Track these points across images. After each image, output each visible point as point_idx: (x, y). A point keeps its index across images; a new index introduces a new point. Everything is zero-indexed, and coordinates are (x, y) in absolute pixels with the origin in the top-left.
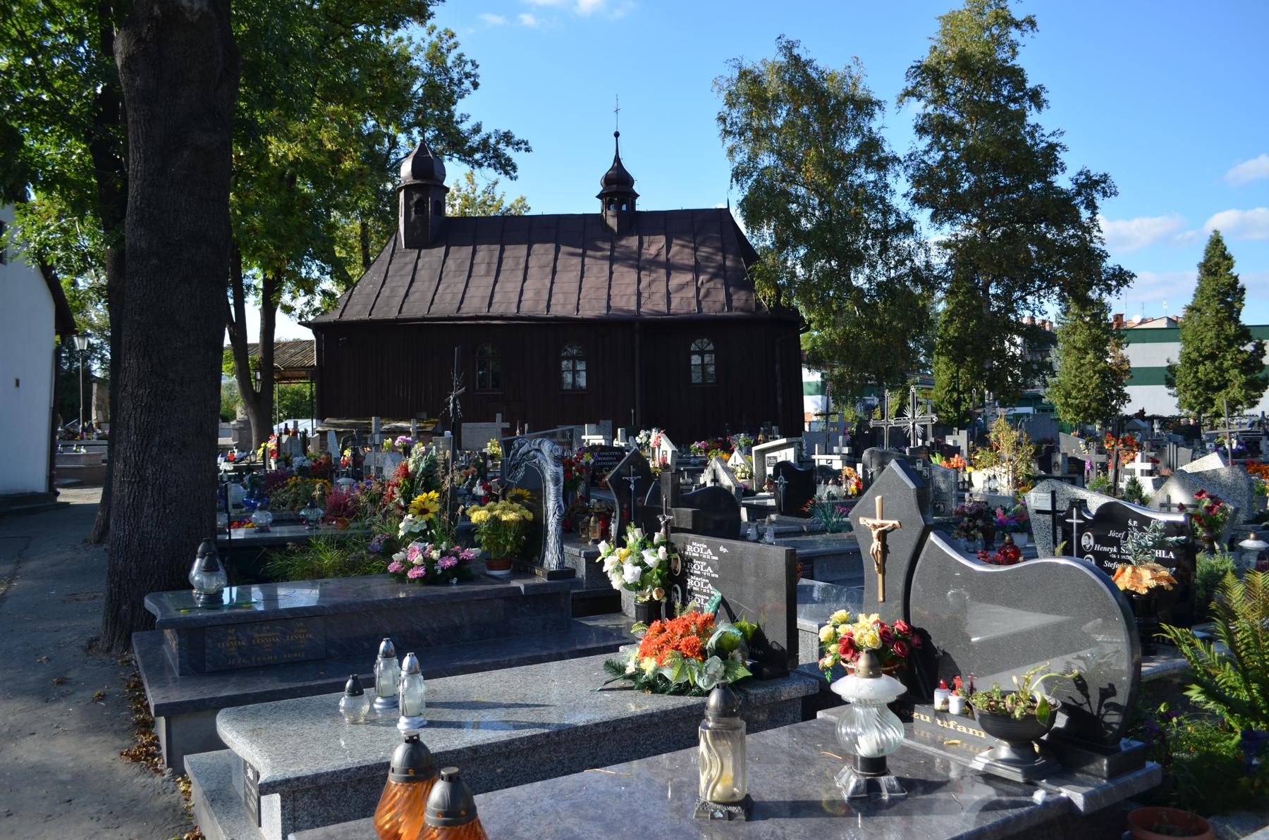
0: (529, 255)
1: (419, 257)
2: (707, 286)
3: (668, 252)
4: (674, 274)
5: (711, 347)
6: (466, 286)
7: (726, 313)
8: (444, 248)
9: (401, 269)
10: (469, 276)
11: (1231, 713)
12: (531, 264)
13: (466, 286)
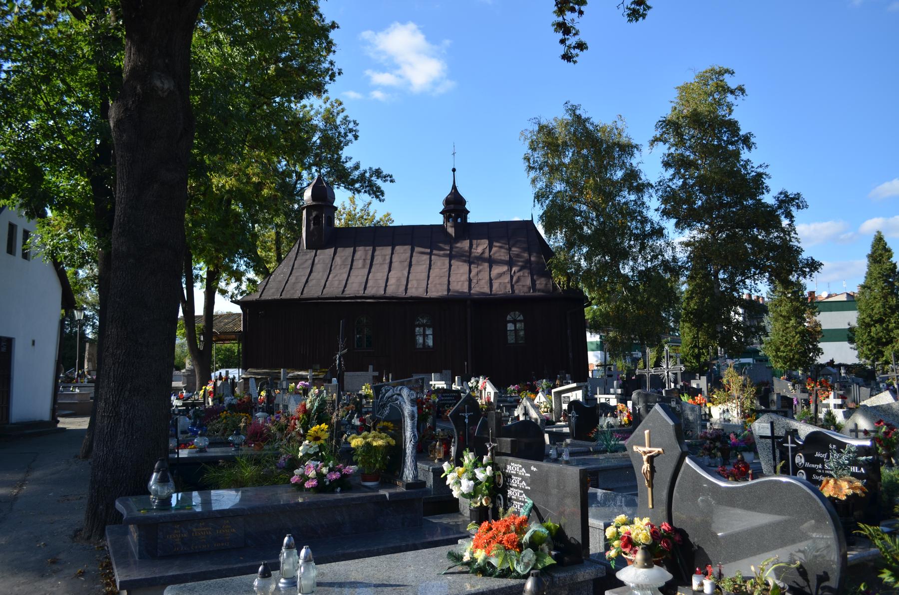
0: (392, 253)
1: (316, 255)
2: (518, 274)
7: (531, 293)
10: (351, 269)
12: (394, 260)
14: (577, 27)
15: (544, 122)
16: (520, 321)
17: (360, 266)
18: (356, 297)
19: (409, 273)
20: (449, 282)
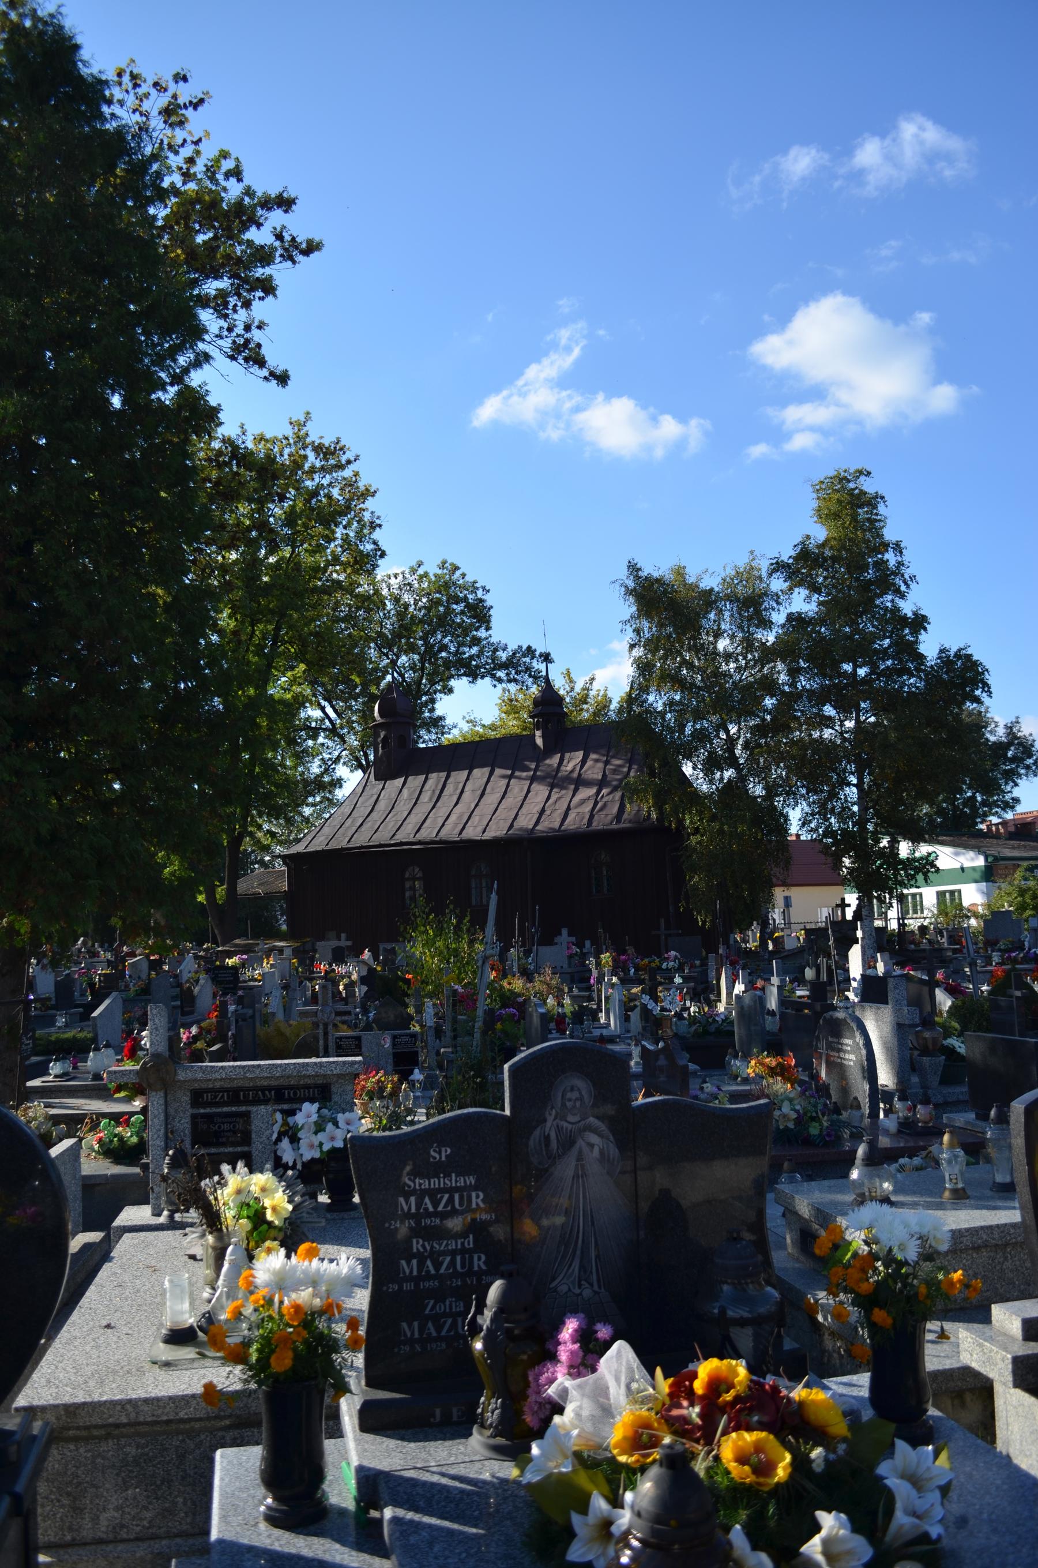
0: (467, 779)
1: (383, 788)
2: (605, 799)
3: (581, 768)
4: (581, 789)
5: (420, 875)
6: (409, 814)
7: (614, 826)
8: (466, 772)
9: (367, 800)
10: (415, 803)
11: (447, 1175)
12: (466, 789)
13: (409, 814)
14: (319, 432)
15: (649, 569)
16: (419, 879)
17: (426, 799)
18: (362, 847)
19: (477, 805)
20: (517, 814)
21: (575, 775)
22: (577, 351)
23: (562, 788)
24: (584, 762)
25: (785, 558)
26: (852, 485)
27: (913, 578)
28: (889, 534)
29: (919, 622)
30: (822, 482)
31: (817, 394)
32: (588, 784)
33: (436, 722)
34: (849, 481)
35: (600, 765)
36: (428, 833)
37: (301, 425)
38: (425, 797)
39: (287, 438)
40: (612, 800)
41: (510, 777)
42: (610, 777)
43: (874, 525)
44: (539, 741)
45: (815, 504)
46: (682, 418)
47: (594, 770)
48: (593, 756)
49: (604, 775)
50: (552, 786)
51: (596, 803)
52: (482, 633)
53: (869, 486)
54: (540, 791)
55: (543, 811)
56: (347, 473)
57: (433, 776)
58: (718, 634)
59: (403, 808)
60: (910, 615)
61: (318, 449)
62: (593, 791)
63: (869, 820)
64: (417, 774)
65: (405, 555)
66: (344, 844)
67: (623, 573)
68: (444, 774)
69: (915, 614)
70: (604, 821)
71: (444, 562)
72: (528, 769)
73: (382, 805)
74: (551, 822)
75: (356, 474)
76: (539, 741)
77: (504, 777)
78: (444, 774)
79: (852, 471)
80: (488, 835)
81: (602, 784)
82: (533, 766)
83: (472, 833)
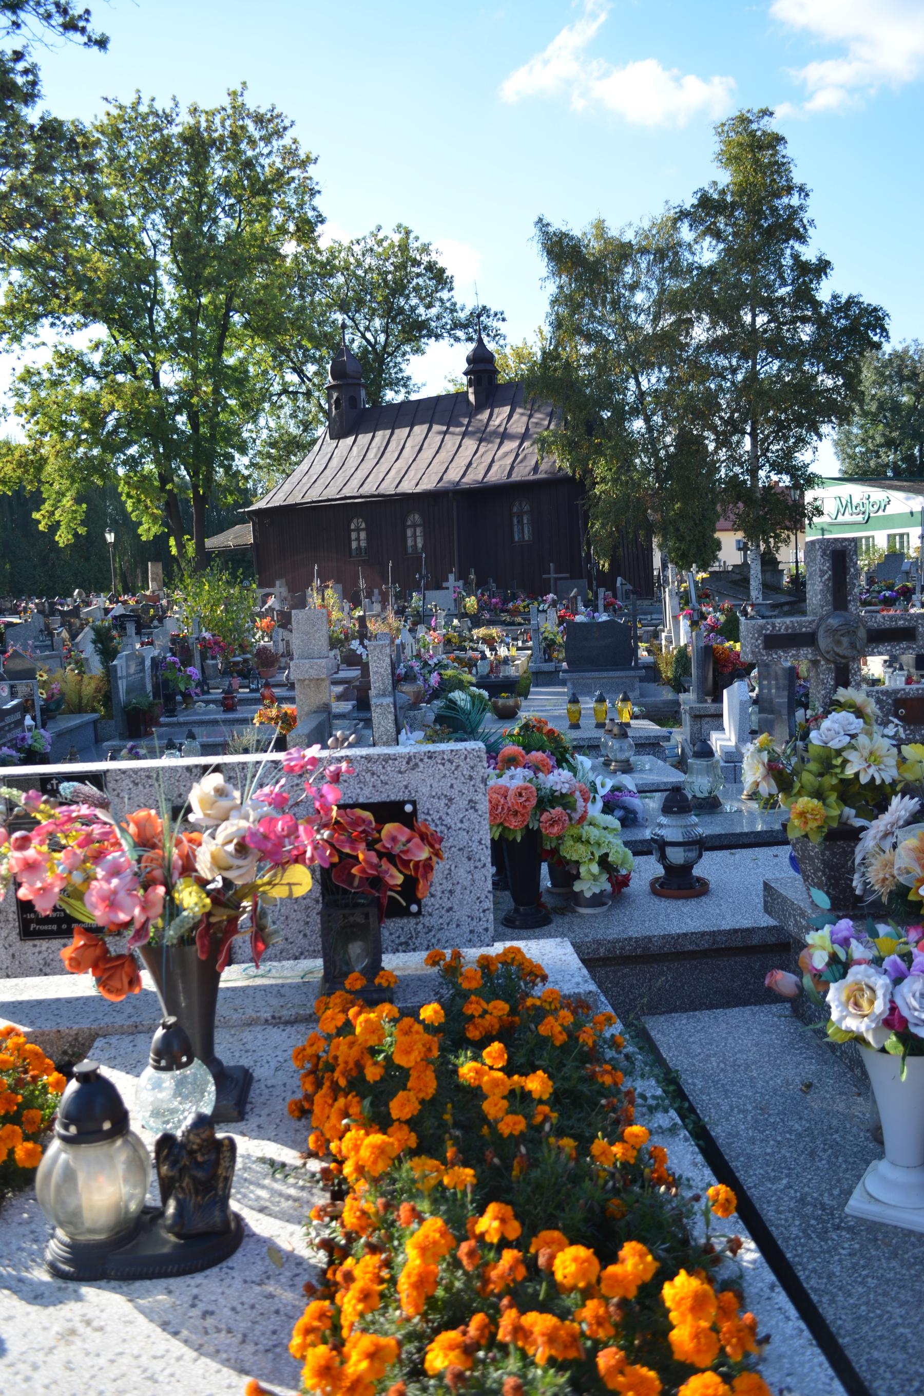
14: (254, 102)
15: (557, 225)
21: (502, 429)
22: (603, 18)
23: (489, 442)
24: (510, 416)
25: (687, 206)
26: (754, 126)
27: (811, 222)
28: (798, 177)
29: (822, 267)
30: (723, 125)
31: (837, 50)
32: (512, 437)
33: (405, 382)
34: (751, 122)
35: (525, 419)
36: (369, 488)
37: (233, 94)
38: (371, 454)
39: (224, 109)
40: (531, 451)
41: (445, 433)
42: (532, 430)
43: (780, 167)
44: (472, 398)
45: (717, 148)
46: (705, 76)
47: (518, 424)
48: (519, 410)
49: (527, 429)
50: (481, 441)
51: (517, 455)
52: (445, 295)
53: (772, 125)
54: (470, 444)
55: (470, 464)
56: (287, 141)
57: (379, 434)
58: (633, 287)
59: (352, 463)
60: (814, 261)
61: (259, 120)
62: (517, 443)
63: (760, 468)
64: (422, 423)
65: (351, 215)
66: (298, 500)
67: (534, 231)
68: (388, 432)
69: (820, 260)
70: (522, 473)
71: (399, 226)
72: (461, 425)
73: (335, 463)
74: (475, 476)
75: (295, 141)
76: (472, 398)
77: (439, 433)
78: (388, 432)
79: (755, 111)
80: (418, 489)
81: (524, 437)
82: (466, 421)
83: (407, 487)
